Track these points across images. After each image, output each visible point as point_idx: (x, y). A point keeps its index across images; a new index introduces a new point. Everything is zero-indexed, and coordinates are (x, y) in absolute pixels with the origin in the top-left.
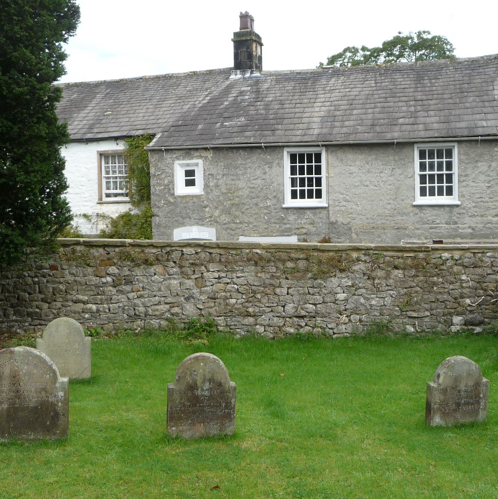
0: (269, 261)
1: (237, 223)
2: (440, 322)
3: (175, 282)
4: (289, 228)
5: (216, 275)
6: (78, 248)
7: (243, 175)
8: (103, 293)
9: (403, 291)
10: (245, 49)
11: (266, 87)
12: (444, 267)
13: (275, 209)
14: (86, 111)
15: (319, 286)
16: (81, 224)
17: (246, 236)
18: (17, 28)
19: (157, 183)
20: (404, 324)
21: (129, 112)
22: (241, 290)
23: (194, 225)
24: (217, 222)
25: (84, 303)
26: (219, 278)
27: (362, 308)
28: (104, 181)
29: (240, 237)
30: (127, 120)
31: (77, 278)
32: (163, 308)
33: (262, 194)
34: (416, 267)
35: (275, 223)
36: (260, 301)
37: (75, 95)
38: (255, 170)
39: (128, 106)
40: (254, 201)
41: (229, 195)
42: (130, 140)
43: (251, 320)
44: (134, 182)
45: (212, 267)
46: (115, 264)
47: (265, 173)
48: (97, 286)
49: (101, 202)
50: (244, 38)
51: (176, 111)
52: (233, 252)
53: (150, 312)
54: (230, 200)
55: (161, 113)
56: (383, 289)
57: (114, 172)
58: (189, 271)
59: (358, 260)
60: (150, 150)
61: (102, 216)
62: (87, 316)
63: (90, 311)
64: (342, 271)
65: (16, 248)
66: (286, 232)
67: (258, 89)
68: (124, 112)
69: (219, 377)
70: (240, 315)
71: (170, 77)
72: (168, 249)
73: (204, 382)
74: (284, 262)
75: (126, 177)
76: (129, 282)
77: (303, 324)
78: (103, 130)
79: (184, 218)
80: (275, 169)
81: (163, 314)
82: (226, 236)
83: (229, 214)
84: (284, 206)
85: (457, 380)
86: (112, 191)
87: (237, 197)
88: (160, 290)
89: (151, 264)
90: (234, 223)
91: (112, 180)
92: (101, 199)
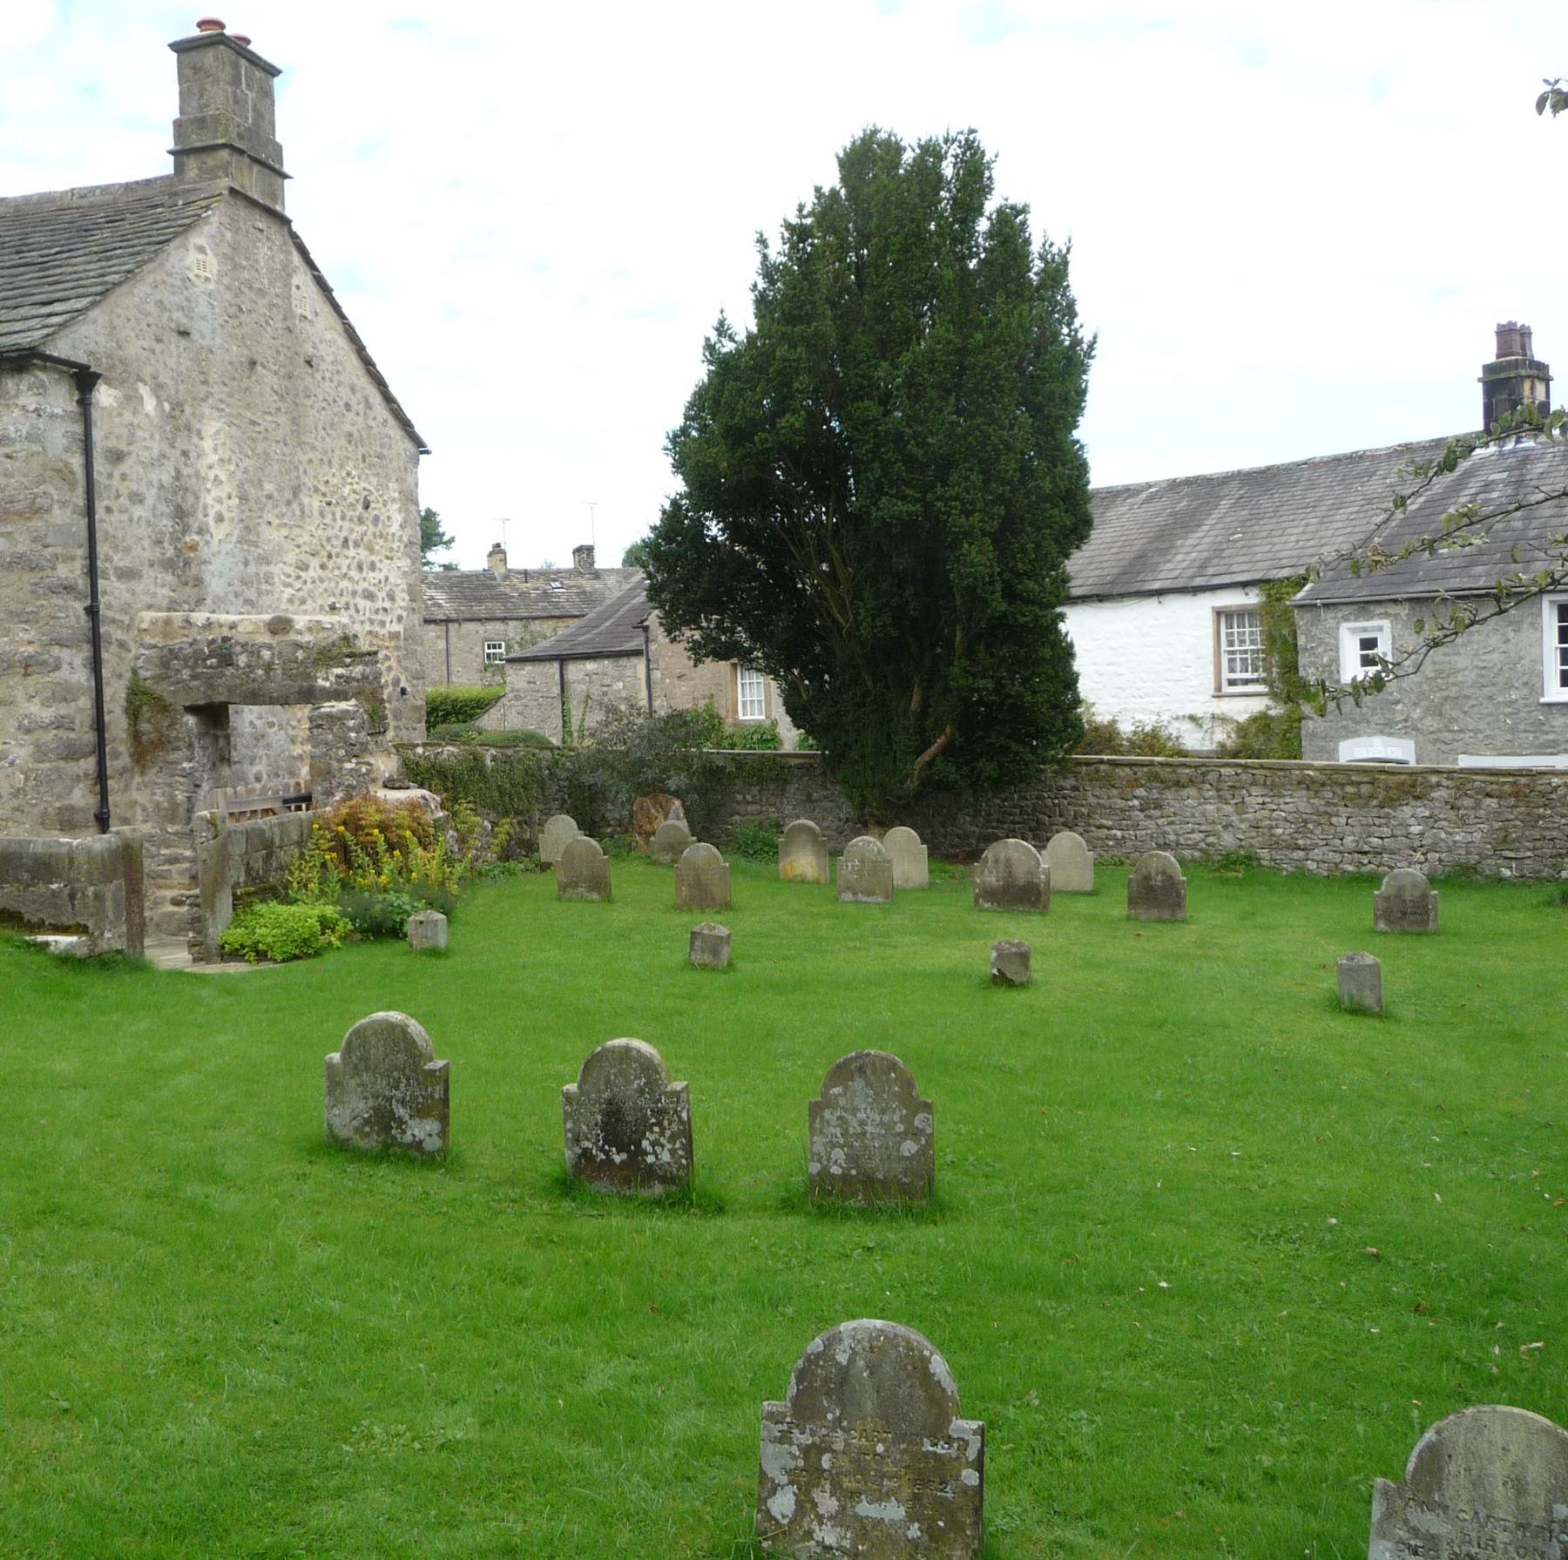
0: (1323, 785)
1: (1453, 731)
2: (1546, 866)
3: (1212, 807)
4: (1554, 741)
5: (1260, 800)
6: (1102, 767)
7: (1464, 645)
8: (1129, 818)
9: (1497, 825)
10: (1505, 396)
11: (1540, 470)
12: (1554, 796)
13: (1526, 705)
14: (1198, 535)
15: (1387, 816)
16: (1185, 731)
17: (1471, 754)
18: (1020, 565)
19: (1311, 662)
20: (1499, 866)
21: (1274, 533)
22: (1289, 818)
23: (1374, 734)
24: (1417, 729)
25: (1109, 828)
26: (1264, 803)
27: (1442, 844)
28: (1225, 658)
29: (1460, 756)
30: (1267, 548)
31: (1101, 801)
32: (1197, 836)
33: (1501, 679)
34: (1516, 795)
35: (1526, 731)
36: (1312, 832)
37: (1184, 503)
38: (1487, 635)
39: (1274, 520)
40: (1486, 690)
41: (1439, 681)
42: (1267, 587)
43: (1301, 854)
44: (1275, 659)
45: (1255, 791)
46: (1142, 786)
47: (1507, 641)
48: (1123, 810)
49: (1219, 694)
50: (1502, 376)
51: (1357, 529)
52: (1280, 773)
53: (1182, 841)
54: (1441, 690)
55: (1329, 533)
56: (1471, 821)
57: (1242, 642)
58: (1227, 794)
59: (1439, 785)
60: (1302, 607)
61: (1221, 719)
62: (1111, 843)
63: (1115, 838)
64: (1417, 798)
65: (1026, 765)
66: (1547, 747)
67: (1522, 475)
68: (1264, 534)
69: (1169, 871)
70: (1288, 847)
71: (1361, 457)
72: (1204, 769)
73: (1157, 874)
74: (1343, 785)
75: (1263, 651)
76: (1158, 806)
77: (1366, 861)
78: (1223, 569)
79: (1357, 723)
80: (1527, 634)
81: (1196, 844)
82: (1433, 755)
83: (1440, 715)
84: (1542, 700)
85: (1401, 889)
86: (1238, 675)
87: (1455, 684)
88: (1193, 816)
89: (1184, 787)
90: (1449, 731)
91: (1238, 656)
92: (1219, 689)
